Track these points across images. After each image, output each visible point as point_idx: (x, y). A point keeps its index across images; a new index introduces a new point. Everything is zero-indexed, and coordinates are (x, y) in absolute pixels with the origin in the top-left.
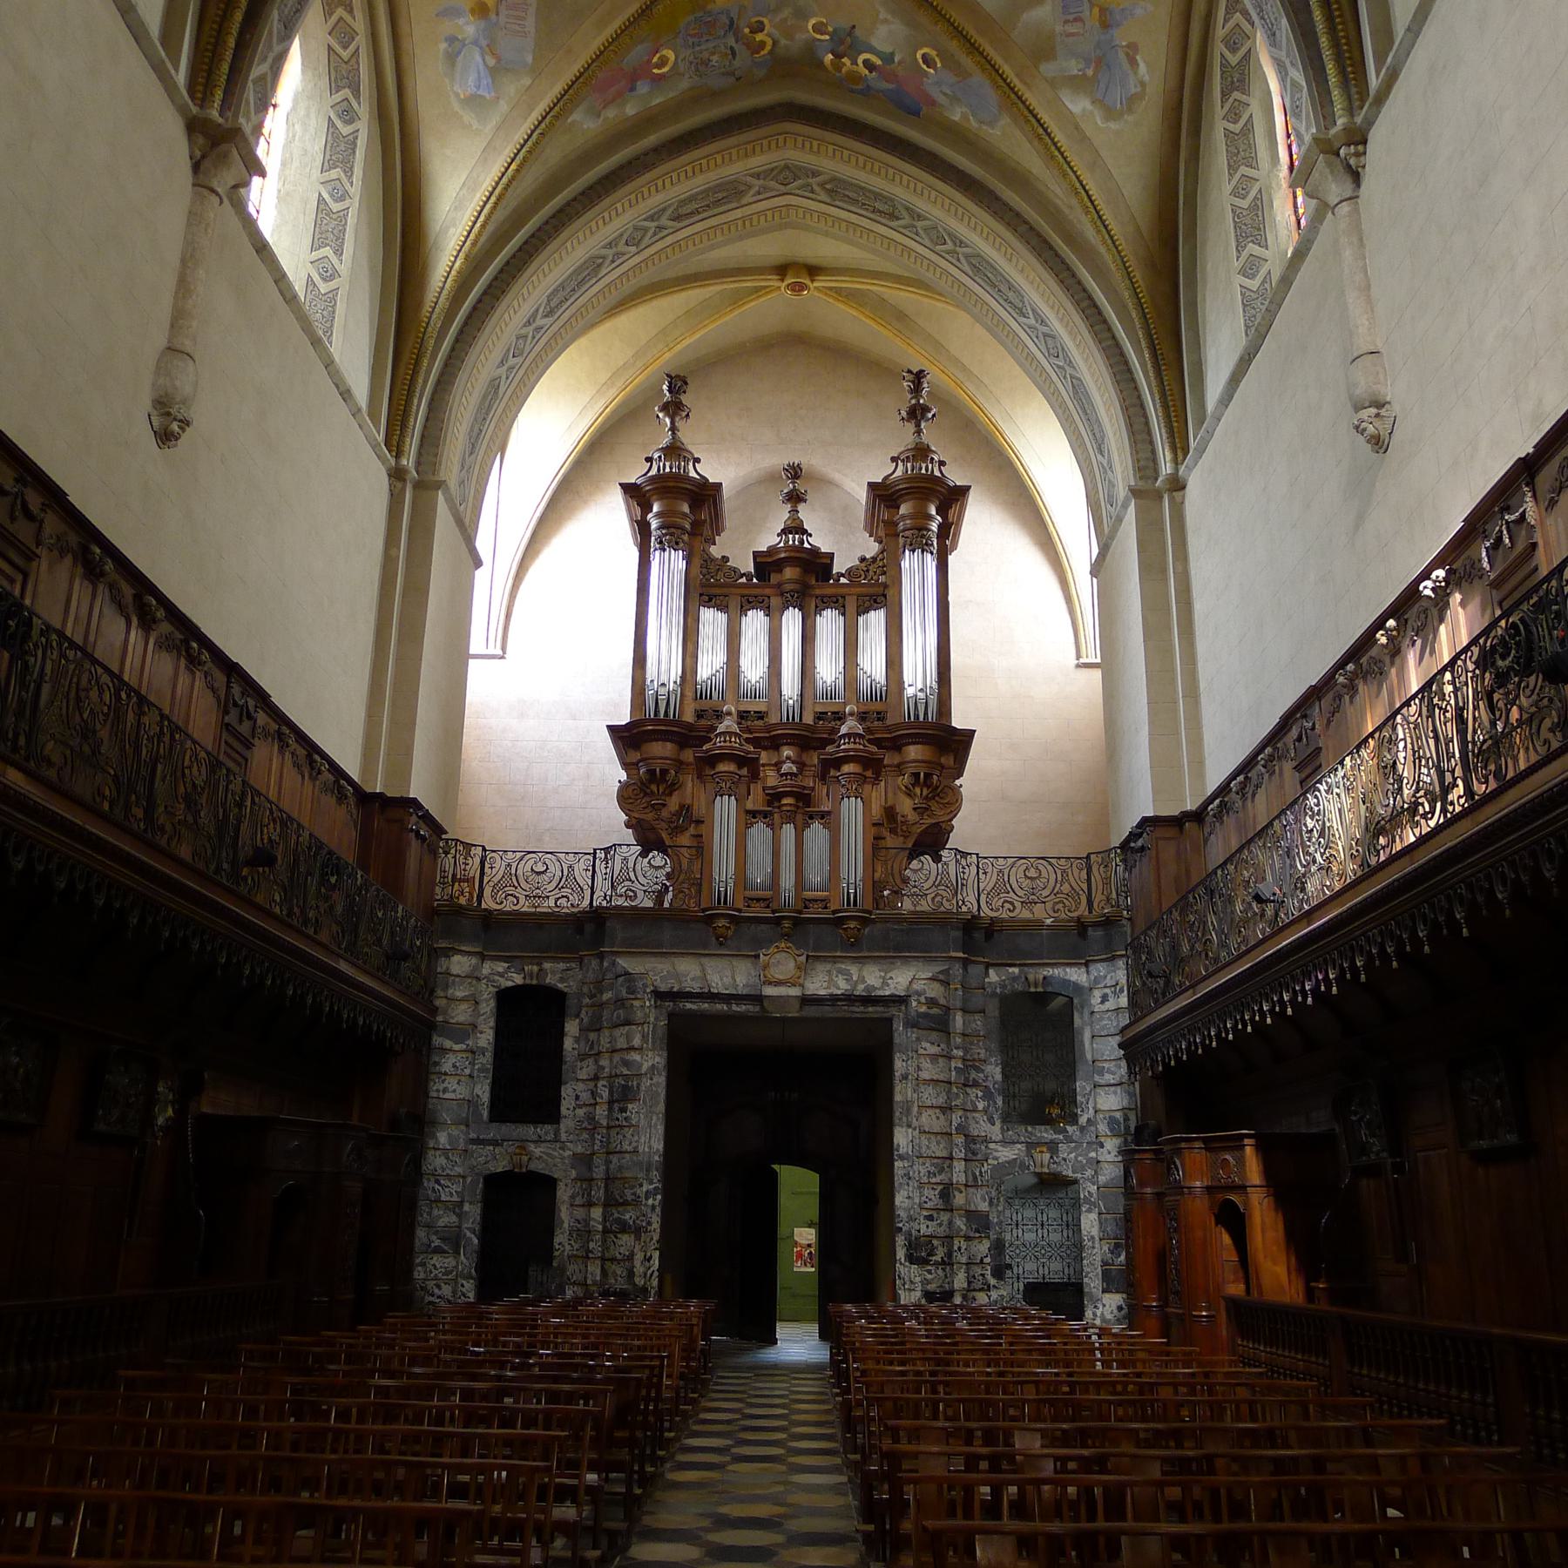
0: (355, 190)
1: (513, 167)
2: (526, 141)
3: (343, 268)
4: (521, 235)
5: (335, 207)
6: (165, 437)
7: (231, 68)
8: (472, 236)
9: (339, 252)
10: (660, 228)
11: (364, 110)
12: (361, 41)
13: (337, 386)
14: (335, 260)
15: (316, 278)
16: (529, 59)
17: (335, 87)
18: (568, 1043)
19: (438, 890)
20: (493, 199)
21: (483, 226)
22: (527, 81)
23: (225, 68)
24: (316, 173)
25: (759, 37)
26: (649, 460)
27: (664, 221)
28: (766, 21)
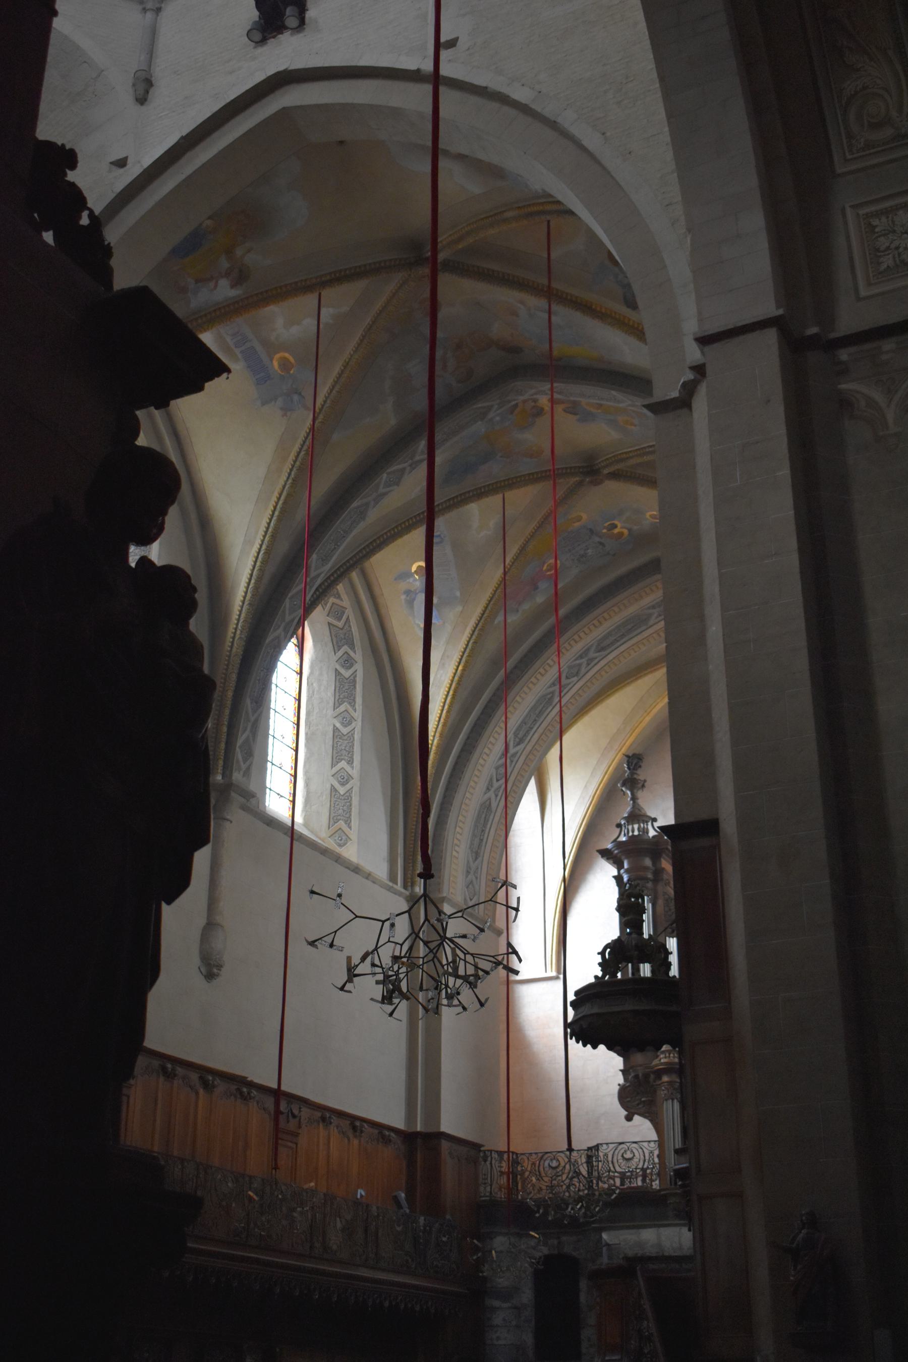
0: (358, 715)
1: (460, 668)
2: (465, 649)
3: (355, 772)
4: (487, 692)
5: (345, 731)
6: (210, 976)
7: (227, 743)
8: (442, 720)
9: (350, 762)
10: (592, 660)
11: (358, 656)
12: (350, 613)
13: (348, 868)
14: (348, 768)
15: (337, 785)
16: (458, 594)
17: (337, 647)
18: (583, 1298)
19: (482, 1189)
20: (451, 692)
21: (448, 712)
22: (459, 608)
23: (223, 745)
24: (330, 712)
25: (616, 531)
26: (619, 826)
27: (592, 654)
28: (616, 522)
